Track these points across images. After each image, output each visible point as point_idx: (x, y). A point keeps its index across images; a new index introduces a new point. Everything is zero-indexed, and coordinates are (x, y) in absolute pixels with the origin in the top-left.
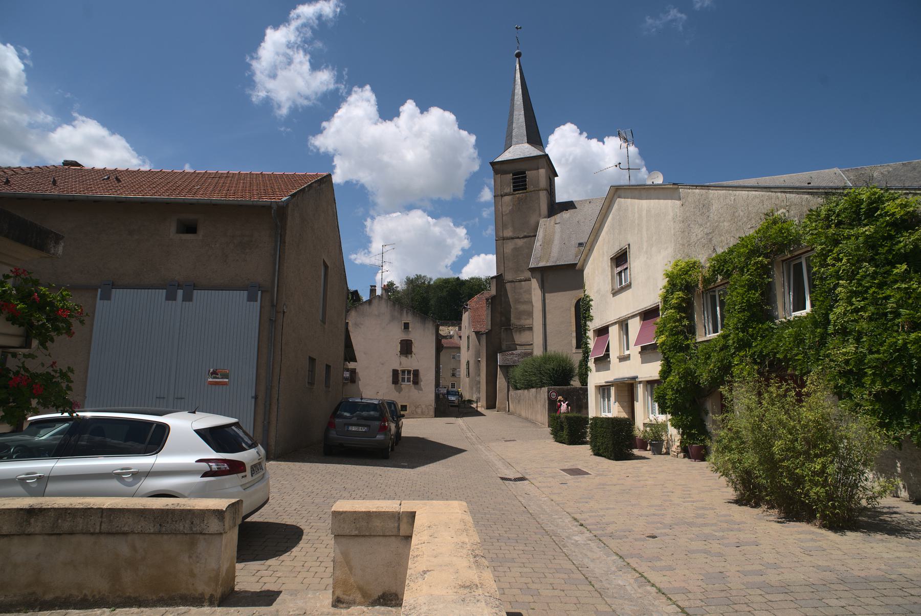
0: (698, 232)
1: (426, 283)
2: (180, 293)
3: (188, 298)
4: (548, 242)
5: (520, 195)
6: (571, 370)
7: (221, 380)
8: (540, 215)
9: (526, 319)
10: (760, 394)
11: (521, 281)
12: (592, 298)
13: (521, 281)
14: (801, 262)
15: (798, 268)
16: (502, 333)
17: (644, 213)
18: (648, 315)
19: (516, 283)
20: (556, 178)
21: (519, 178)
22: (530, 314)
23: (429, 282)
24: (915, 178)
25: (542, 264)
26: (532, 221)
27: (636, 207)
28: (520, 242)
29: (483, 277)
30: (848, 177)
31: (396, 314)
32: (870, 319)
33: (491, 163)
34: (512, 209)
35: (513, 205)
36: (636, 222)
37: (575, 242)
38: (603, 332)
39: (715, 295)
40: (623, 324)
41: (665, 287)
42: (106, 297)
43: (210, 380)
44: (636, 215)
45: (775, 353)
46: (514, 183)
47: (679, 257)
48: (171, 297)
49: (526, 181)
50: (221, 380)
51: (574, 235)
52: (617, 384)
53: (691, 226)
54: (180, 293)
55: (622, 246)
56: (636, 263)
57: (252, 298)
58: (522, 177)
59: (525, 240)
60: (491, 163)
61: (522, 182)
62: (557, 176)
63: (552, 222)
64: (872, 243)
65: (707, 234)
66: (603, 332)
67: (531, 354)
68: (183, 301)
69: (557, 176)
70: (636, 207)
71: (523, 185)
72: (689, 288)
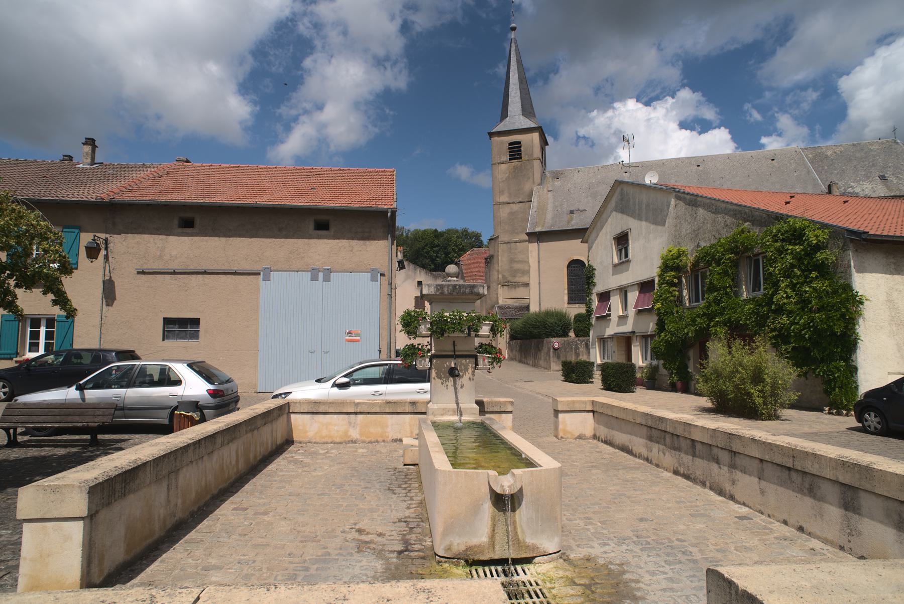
0: (686, 229)
1: (404, 234)
2: (321, 275)
3: (327, 279)
4: (542, 209)
5: (515, 163)
6: (569, 324)
7: (355, 338)
8: (534, 182)
9: (521, 277)
10: (730, 347)
11: (516, 242)
12: (595, 267)
13: (516, 242)
14: (759, 259)
15: (757, 261)
16: (499, 289)
17: (644, 206)
18: (645, 286)
19: (512, 244)
20: (546, 147)
21: (514, 148)
22: (527, 272)
23: (407, 234)
24: (862, 158)
25: (538, 229)
26: (527, 187)
27: (637, 200)
28: (515, 207)
29: (459, 229)
30: (807, 155)
31: (410, 273)
32: (796, 303)
33: (489, 133)
34: (509, 176)
35: (510, 172)
36: (637, 212)
37: (566, 209)
38: (605, 297)
39: (698, 275)
40: (623, 291)
41: (660, 267)
42: (267, 278)
43: (347, 338)
44: (637, 207)
45: (739, 321)
46: (510, 152)
47: (670, 247)
48: (314, 278)
49: (521, 150)
50: (355, 338)
51: (566, 203)
52: (618, 337)
53: (682, 222)
54: (321, 275)
55: (624, 229)
56: (633, 246)
57: (373, 279)
58: (517, 147)
59: (521, 205)
60: (489, 133)
61: (518, 151)
62: (548, 145)
63: (545, 190)
64: (799, 258)
65: (694, 231)
66: (605, 297)
67: (528, 308)
68: (324, 281)
69: (548, 145)
70: (637, 200)
71: (518, 155)
72: (678, 269)
